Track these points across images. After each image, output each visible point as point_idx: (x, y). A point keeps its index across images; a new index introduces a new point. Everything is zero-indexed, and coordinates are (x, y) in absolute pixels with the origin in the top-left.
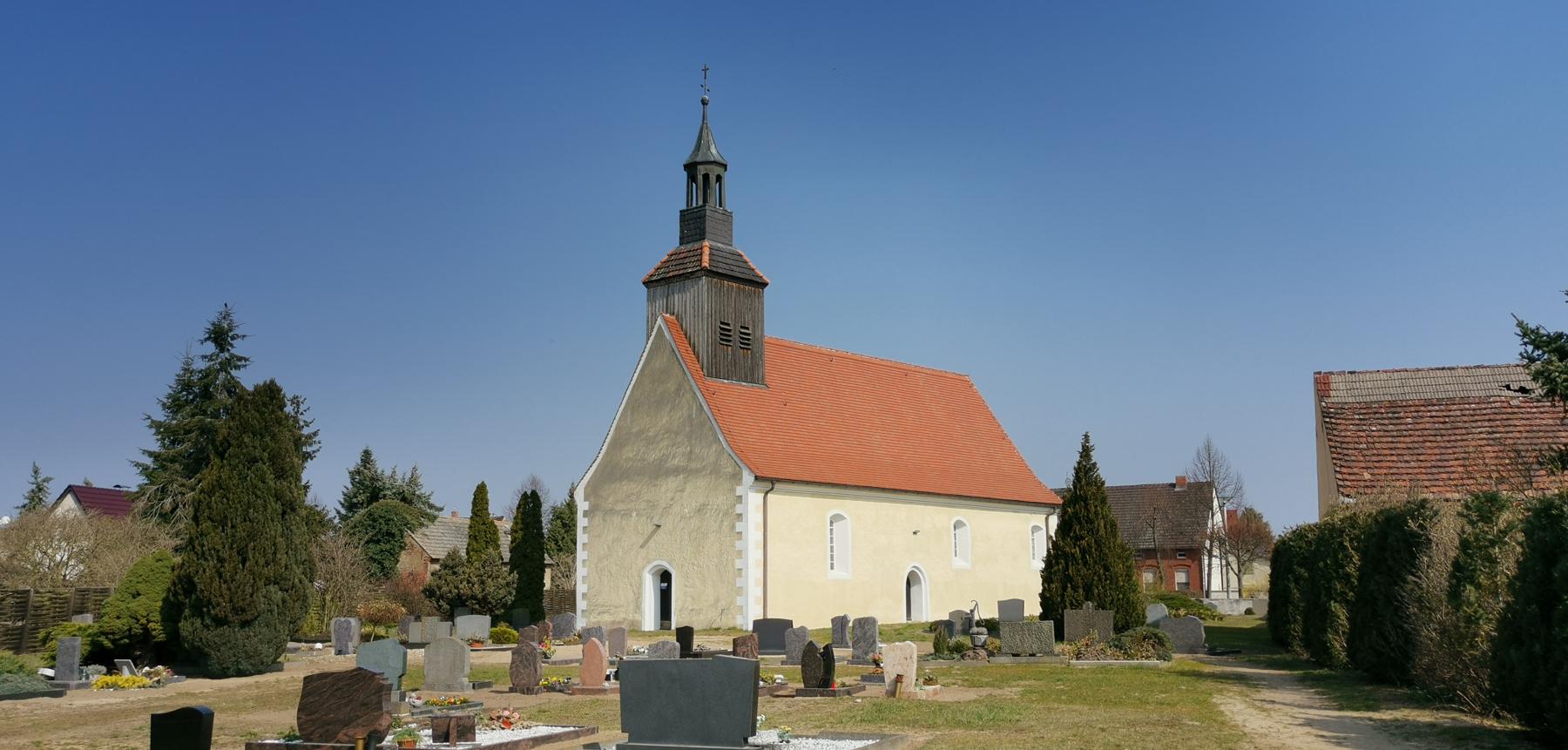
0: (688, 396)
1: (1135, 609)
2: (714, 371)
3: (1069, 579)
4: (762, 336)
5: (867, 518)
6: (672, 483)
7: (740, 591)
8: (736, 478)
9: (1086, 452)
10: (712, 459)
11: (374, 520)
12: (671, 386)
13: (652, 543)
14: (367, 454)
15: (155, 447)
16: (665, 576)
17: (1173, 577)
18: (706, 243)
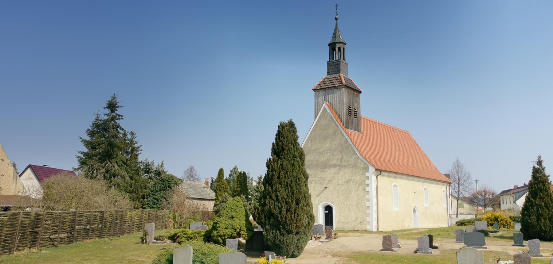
3: (541, 215)
6: (332, 171)
7: (368, 215)
8: (366, 169)
11: (163, 182)
13: (322, 195)
15: (86, 150)
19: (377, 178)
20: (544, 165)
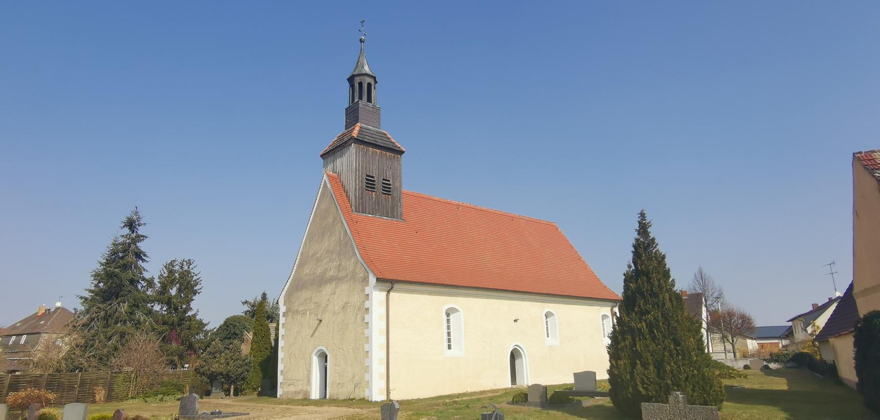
0: (339, 225)
2: (361, 208)
4: (400, 186)
5: (474, 310)
6: (328, 289)
7: (367, 369)
8: (365, 280)
9: (643, 229)
12: (330, 220)
14: (264, 295)
18: (358, 124)
19: (387, 296)
20: (653, 232)
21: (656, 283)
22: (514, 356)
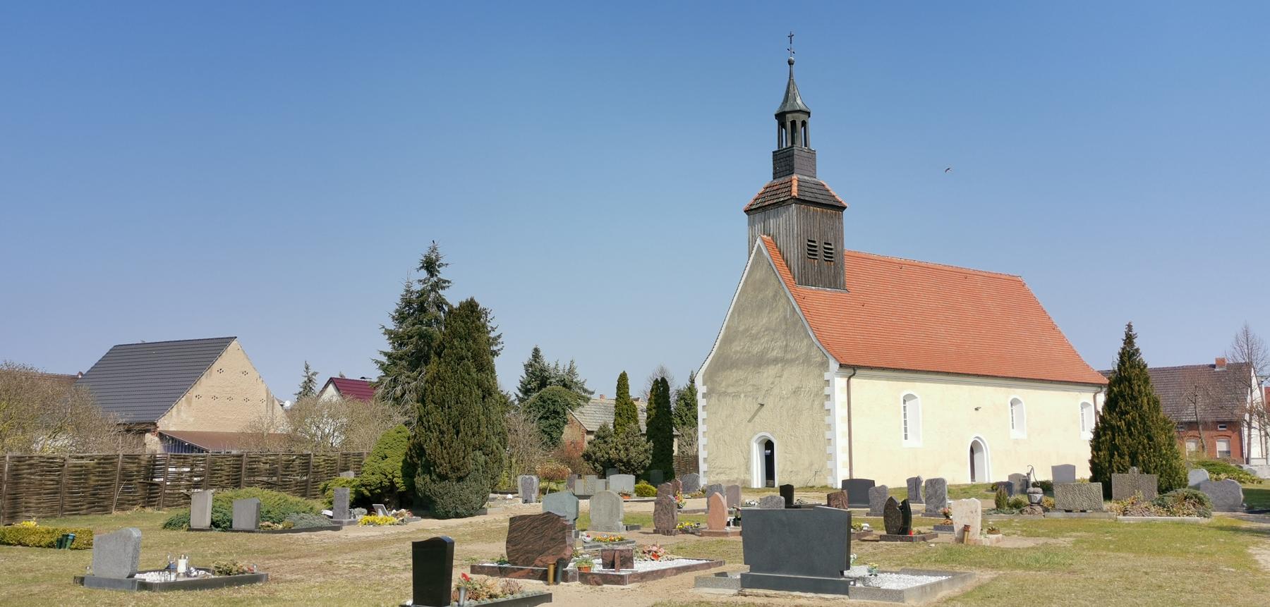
0: (783, 301)
1: (1177, 474)
2: (804, 280)
3: (1116, 448)
4: (843, 250)
5: (934, 396)
6: (772, 370)
7: (831, 457)
8: (824, 365)
9: (1129, 339)
10: (804, 351)
12: (770, 293)
13: (757, 419)
14: (536, 351)
15: (389, 349)
16: (769, 445)
17: (1215, 446)
18: (795, 177)
20: (1138, 343)
21: (1136, 388)
22: (974, 449)
